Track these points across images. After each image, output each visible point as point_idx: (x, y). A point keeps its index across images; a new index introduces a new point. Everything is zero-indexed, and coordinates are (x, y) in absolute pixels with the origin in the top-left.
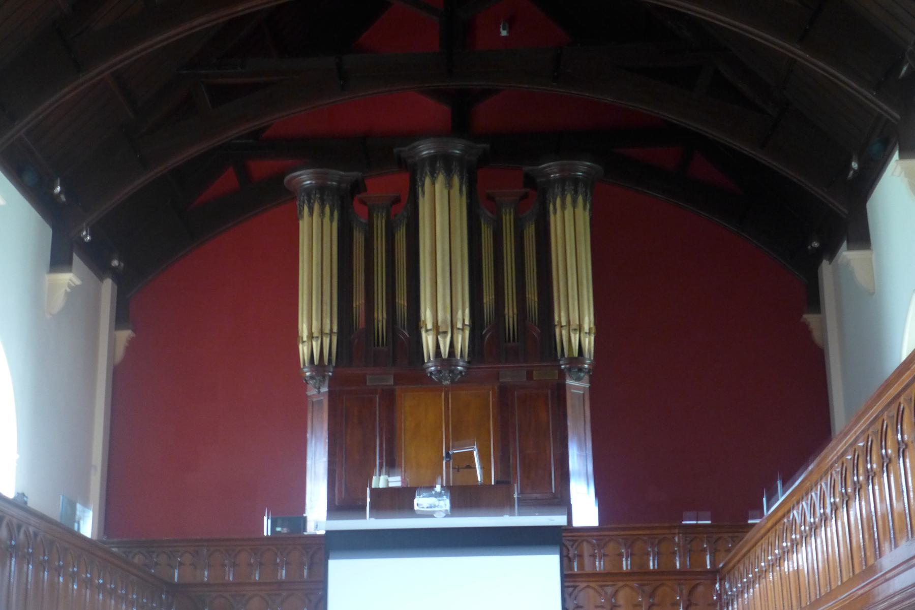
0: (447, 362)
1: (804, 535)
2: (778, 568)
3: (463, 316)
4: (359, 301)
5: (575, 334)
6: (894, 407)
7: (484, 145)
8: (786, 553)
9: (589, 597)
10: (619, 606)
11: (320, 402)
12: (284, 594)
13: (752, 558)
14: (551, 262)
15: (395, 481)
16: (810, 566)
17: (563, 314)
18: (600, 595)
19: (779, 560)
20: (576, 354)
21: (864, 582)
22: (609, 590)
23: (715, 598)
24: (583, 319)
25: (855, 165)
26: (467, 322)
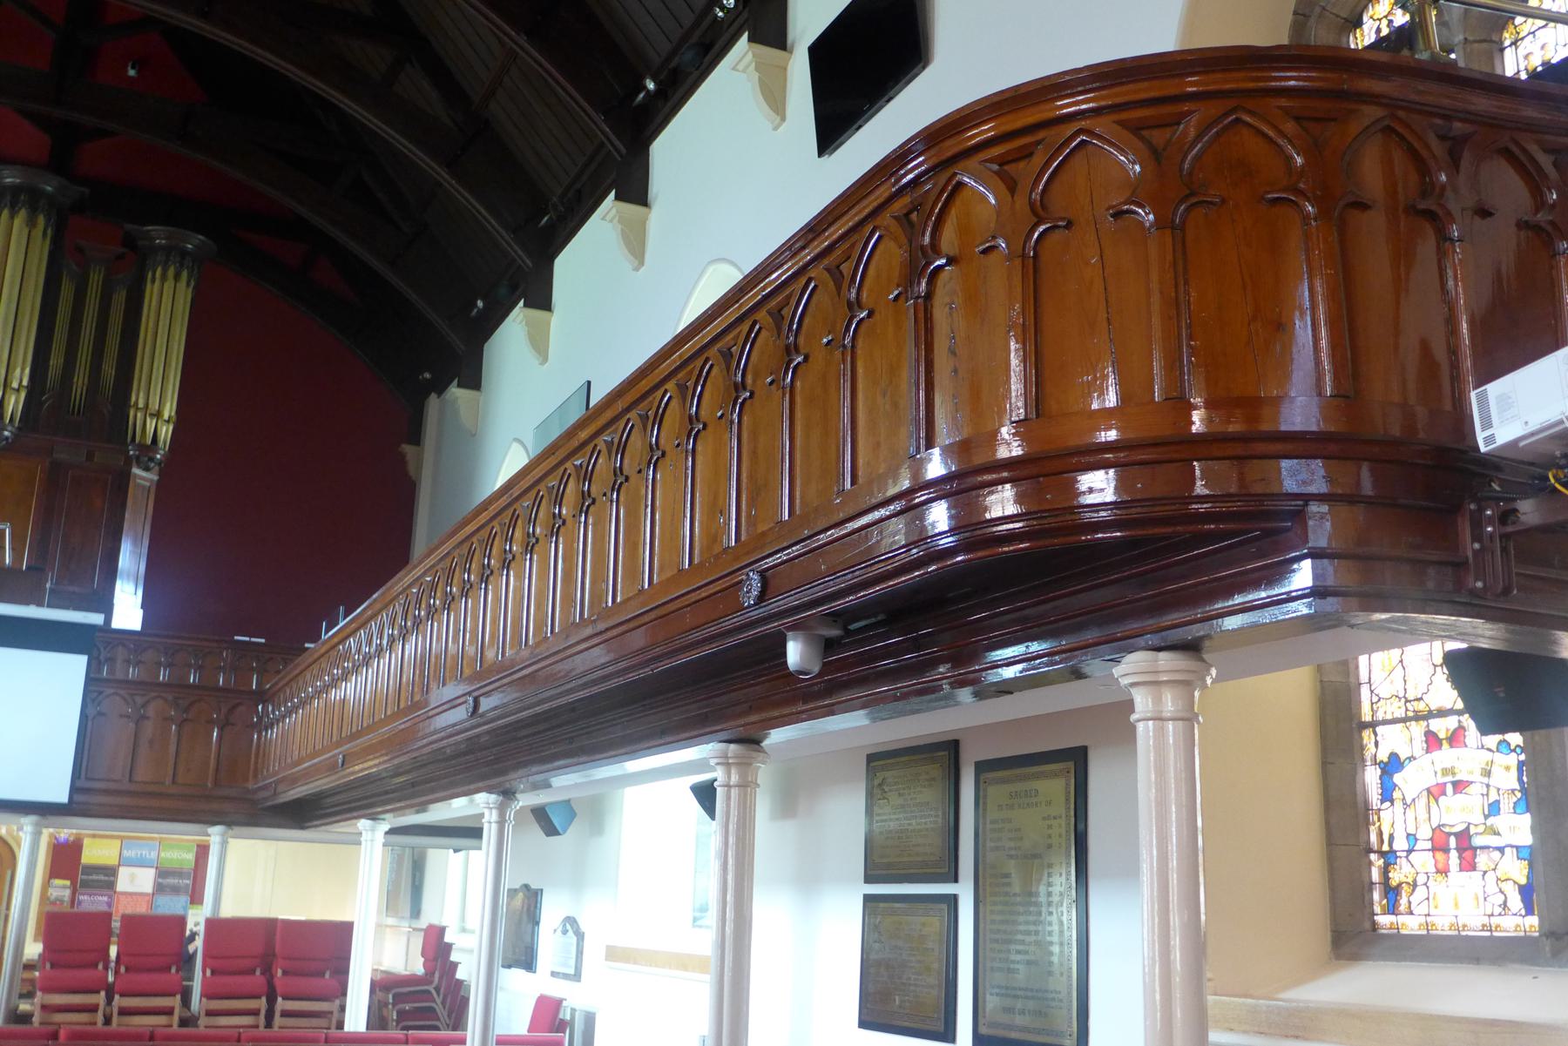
1: (357, 664)
2: (325, 695)
5: (152, 419)
6: (466, 547)
7: (82, 189)
8: (335, 683)
10: (148, 718)
13: (301, 683)
14: (143, 302)
16: (357, 696)
18: (128, 704)
19: (326, 688)
20: (149, 441)
21: (406, 717)
22: (139, 700)
23: (255, 720)
24: (164, 405)
25: (480, 304)
26: (25, 383)
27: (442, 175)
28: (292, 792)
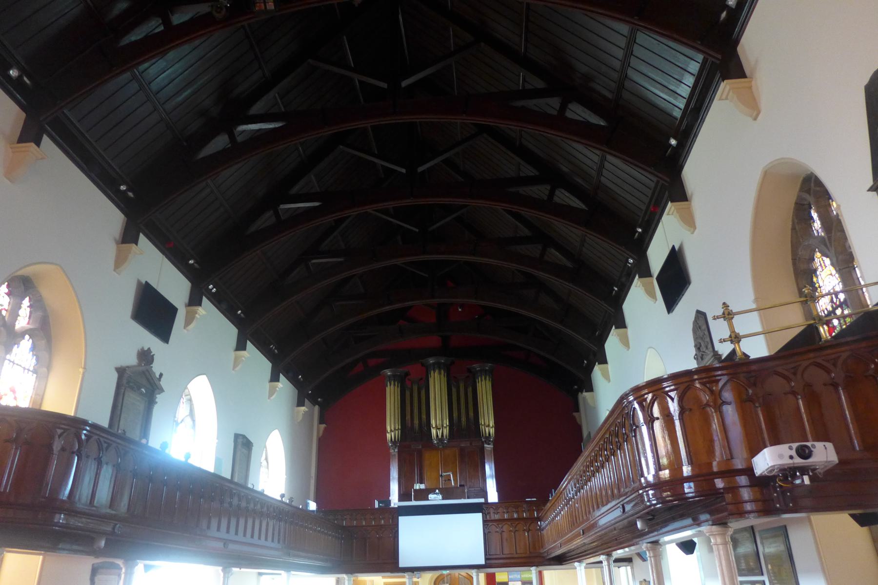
0: (441, 440)
3: (446, 422)
4: (408, 417)
9: (493, 528)
11: (395, 455)
12: (384, 529)
15: (423, 486)
17: (482, 420)
18: (497, 528)
20: (488, 435)
25: (585, 362)
26: (448, 424)
27: (559, 326)
28: (558, 552)
